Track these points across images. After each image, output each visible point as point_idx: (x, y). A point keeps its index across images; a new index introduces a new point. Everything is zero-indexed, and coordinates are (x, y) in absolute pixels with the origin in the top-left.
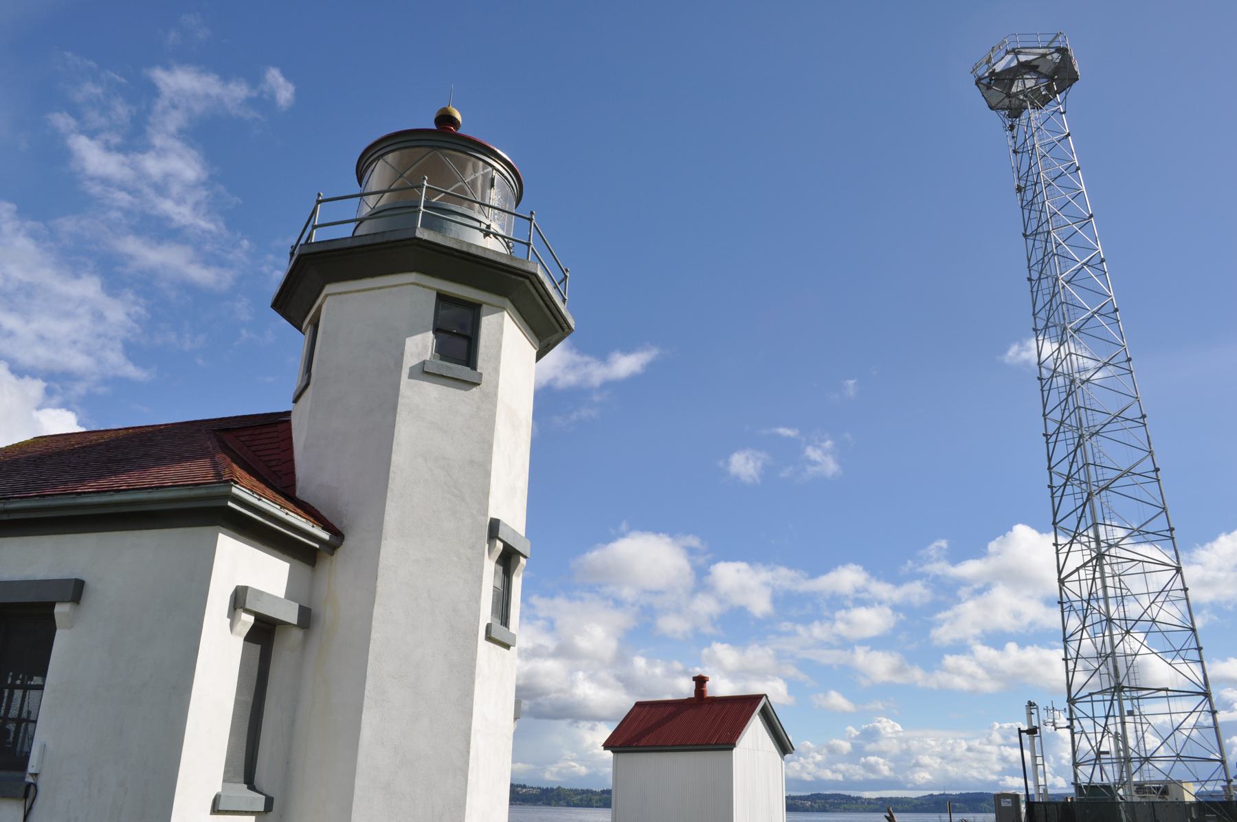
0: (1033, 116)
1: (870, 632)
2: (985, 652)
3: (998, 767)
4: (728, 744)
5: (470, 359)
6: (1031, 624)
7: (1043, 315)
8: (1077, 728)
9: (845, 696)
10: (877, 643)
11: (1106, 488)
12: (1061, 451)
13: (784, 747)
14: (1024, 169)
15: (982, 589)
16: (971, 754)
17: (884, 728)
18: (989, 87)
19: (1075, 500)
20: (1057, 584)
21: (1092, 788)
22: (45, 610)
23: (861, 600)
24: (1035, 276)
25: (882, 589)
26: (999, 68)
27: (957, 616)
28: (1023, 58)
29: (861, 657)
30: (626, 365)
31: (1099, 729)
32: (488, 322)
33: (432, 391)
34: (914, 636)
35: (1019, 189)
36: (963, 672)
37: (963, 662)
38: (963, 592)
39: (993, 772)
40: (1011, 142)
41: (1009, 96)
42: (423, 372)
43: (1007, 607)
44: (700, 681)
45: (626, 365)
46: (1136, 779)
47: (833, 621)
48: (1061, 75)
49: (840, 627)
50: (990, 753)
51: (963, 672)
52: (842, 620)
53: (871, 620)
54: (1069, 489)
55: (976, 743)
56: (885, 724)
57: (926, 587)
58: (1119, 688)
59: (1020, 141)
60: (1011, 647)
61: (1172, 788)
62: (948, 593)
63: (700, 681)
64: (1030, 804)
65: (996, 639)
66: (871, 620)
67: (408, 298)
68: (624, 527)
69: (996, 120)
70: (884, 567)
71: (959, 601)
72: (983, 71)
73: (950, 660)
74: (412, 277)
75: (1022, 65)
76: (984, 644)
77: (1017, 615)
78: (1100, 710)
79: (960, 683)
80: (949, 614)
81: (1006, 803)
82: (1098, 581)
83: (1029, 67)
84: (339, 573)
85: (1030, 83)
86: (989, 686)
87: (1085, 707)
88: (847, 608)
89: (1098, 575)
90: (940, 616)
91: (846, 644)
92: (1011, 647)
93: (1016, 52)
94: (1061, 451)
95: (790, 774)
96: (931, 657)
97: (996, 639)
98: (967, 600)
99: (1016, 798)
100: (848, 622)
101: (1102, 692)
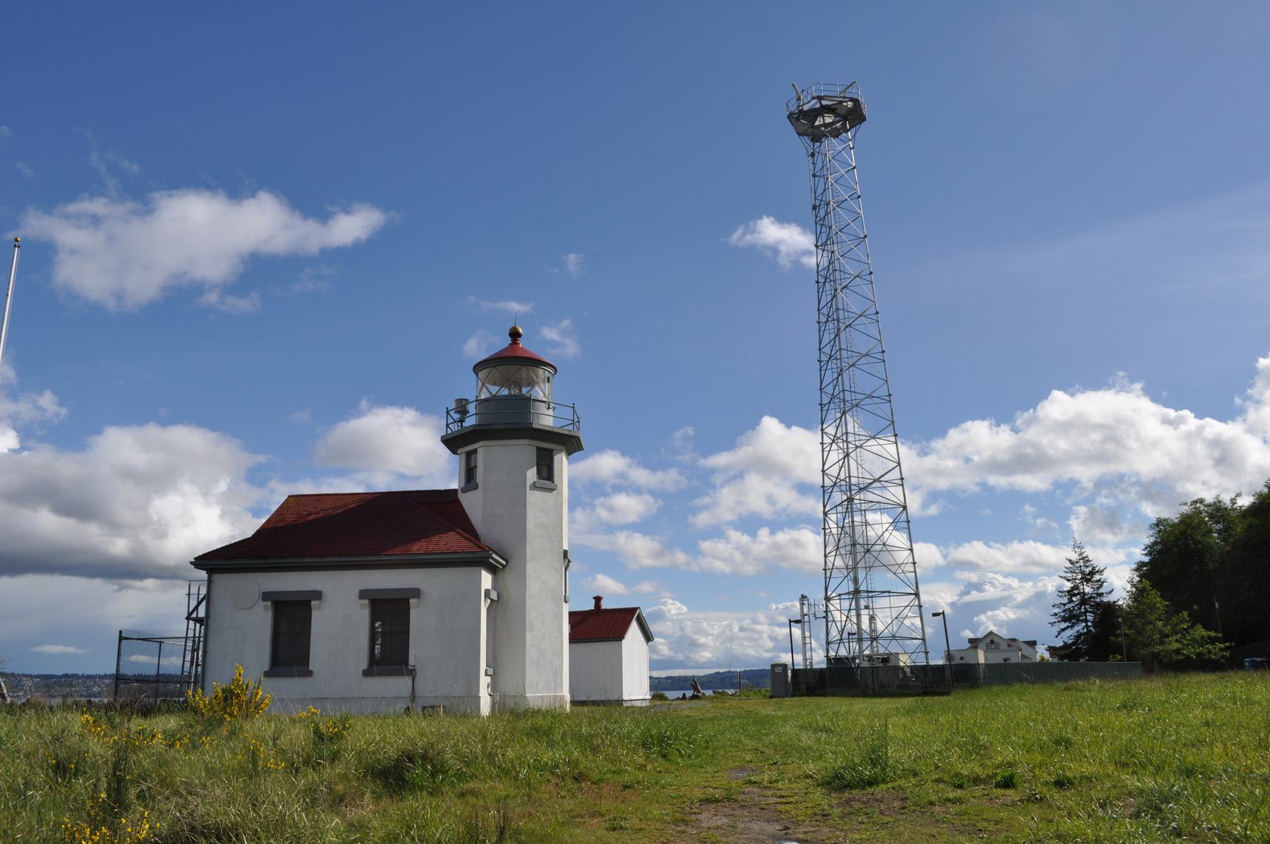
0: (831, 145)
1: (632, 518)
2: (736, 536)
3: (770, 644)
4: (620, 636)
5: (550, 477)
6: (785, 510)
7: (827, 350)
8: (830, 619)
9: (612, 576)
10: (643, 527)
11: (861, 447)
12: (829, 377)
13: (648, 637)
14: (820, 191)
15: (737, 476)
16: (742, 634)
17: (669, 611)
18: (797, 119)
19: (835, 397)
20: (822, 515)
21: (839, 660)
22: (406, 602)
23: (622, 485)
24: (821, 280)
25: (641, 476)
26: (806, 108)
27: (715, 504)
28: (824, 103)
29: (621, 538)
30: (351, 227)
31: (844, 618)
32: (556, 458)
33: (538, 494)
34: (674, 519)
35: (814, 208)
36: (721, 554)
37: (721, 547)
38: (718, 479)
39: (767, 651)
40: (812, 167)
41: (813, 127)
42: (534, 487)
43: (757, 493)
44: (598, 600)
45: (351, 227)
46: (867, 652)
47: (593, 508)
48: (854, 116)
49: (603, 514)
50: (761, 632)
51: (721, 554)
52: (603, 505)
53: (629, 506)
54: (832, 406)
55: (746, 623)
56: (669, 607)
57: (681, 474)
58: (857, 592)
59: (819, 166)
60: (764, 533)
61: (892, 658)
62: (704, 482)
63: (598, 600)
64: (794, 671)
65: (750, 524)
66: (629, 506)
67: (524, 450)
68: (364, 404)
69: (801, 145)
70: (644, 451)
71: (714, 487)
72: (793, 108)
73: (706, 545)
74: (527, 441)
75: (823, 107)
76: (737, 530)
77: (770, 499)
78: (846, 604)
79: (720, 566)
80: (707, 500)
81: (778, 670)
82: (853, 613)
83: (829, 110)
84: (509, 578)
85: (828, 120)
86: (749, 569)
87: (836, 602)
88: (607, 495)
89: (853, 606)
90: (698, 502)
91: (609, 529)
92: (764, 533)
93: (820, 98)
94: (829, 377)
95: (655, 657)
96: (689, 541)
97: (750, 524)
98: (722, 486)
99: (785, 666)
100: (611, 509)
101: (849, 593)
